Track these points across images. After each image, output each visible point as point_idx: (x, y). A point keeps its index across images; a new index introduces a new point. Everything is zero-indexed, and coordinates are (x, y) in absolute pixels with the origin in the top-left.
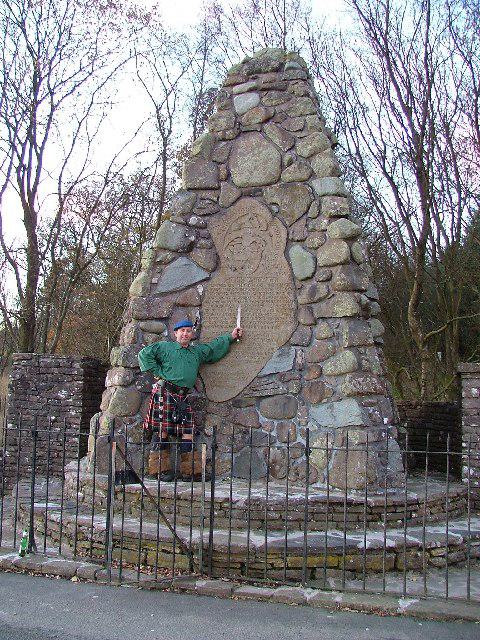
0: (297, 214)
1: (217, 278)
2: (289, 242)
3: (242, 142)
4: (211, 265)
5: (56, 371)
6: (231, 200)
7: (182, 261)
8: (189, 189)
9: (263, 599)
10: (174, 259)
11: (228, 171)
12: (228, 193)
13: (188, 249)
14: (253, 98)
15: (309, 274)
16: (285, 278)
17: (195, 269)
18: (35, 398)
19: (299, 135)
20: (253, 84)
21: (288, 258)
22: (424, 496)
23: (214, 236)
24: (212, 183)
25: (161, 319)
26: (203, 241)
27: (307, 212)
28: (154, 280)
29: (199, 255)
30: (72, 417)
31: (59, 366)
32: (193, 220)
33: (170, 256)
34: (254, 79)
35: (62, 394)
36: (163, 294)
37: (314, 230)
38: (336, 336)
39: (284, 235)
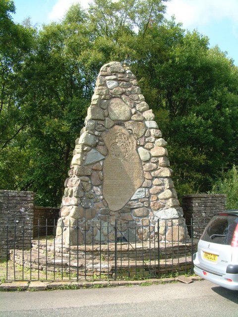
0: (141, 134)
1: (108, 159)
2: (138, 146)
3: (113, 101)
4: (105, 153)
5: (19, 198)
6: (111, 126)
7: (93, 151)
8: (93, 119)
9: (135, 284)
10: (90, 150)
11: (108, 113)
12: (108, 123)
13: (95, 146)
14: (115, 83)
15: (147, 159)
16: (137, 161)
17: (99, 154)
18: (7, 212)
19: (136, 102)
20: (114, 77)
21: (138, 152)
22: (33, 274)
23: (105, 140)
24: (102, 118)
25: (88, 176)
26: (101, 143)
27: (144, 134)
28: (84, 159)
29: (101, 148)
30: (28, 220)
31: (19, 196)
32: (96, 133)
33: (89, 148)
34: (115, 75)
35: (22, 210)
36: (87, 165)
37: (148, 142)
38: (163, 184)
39: (135, 143)
